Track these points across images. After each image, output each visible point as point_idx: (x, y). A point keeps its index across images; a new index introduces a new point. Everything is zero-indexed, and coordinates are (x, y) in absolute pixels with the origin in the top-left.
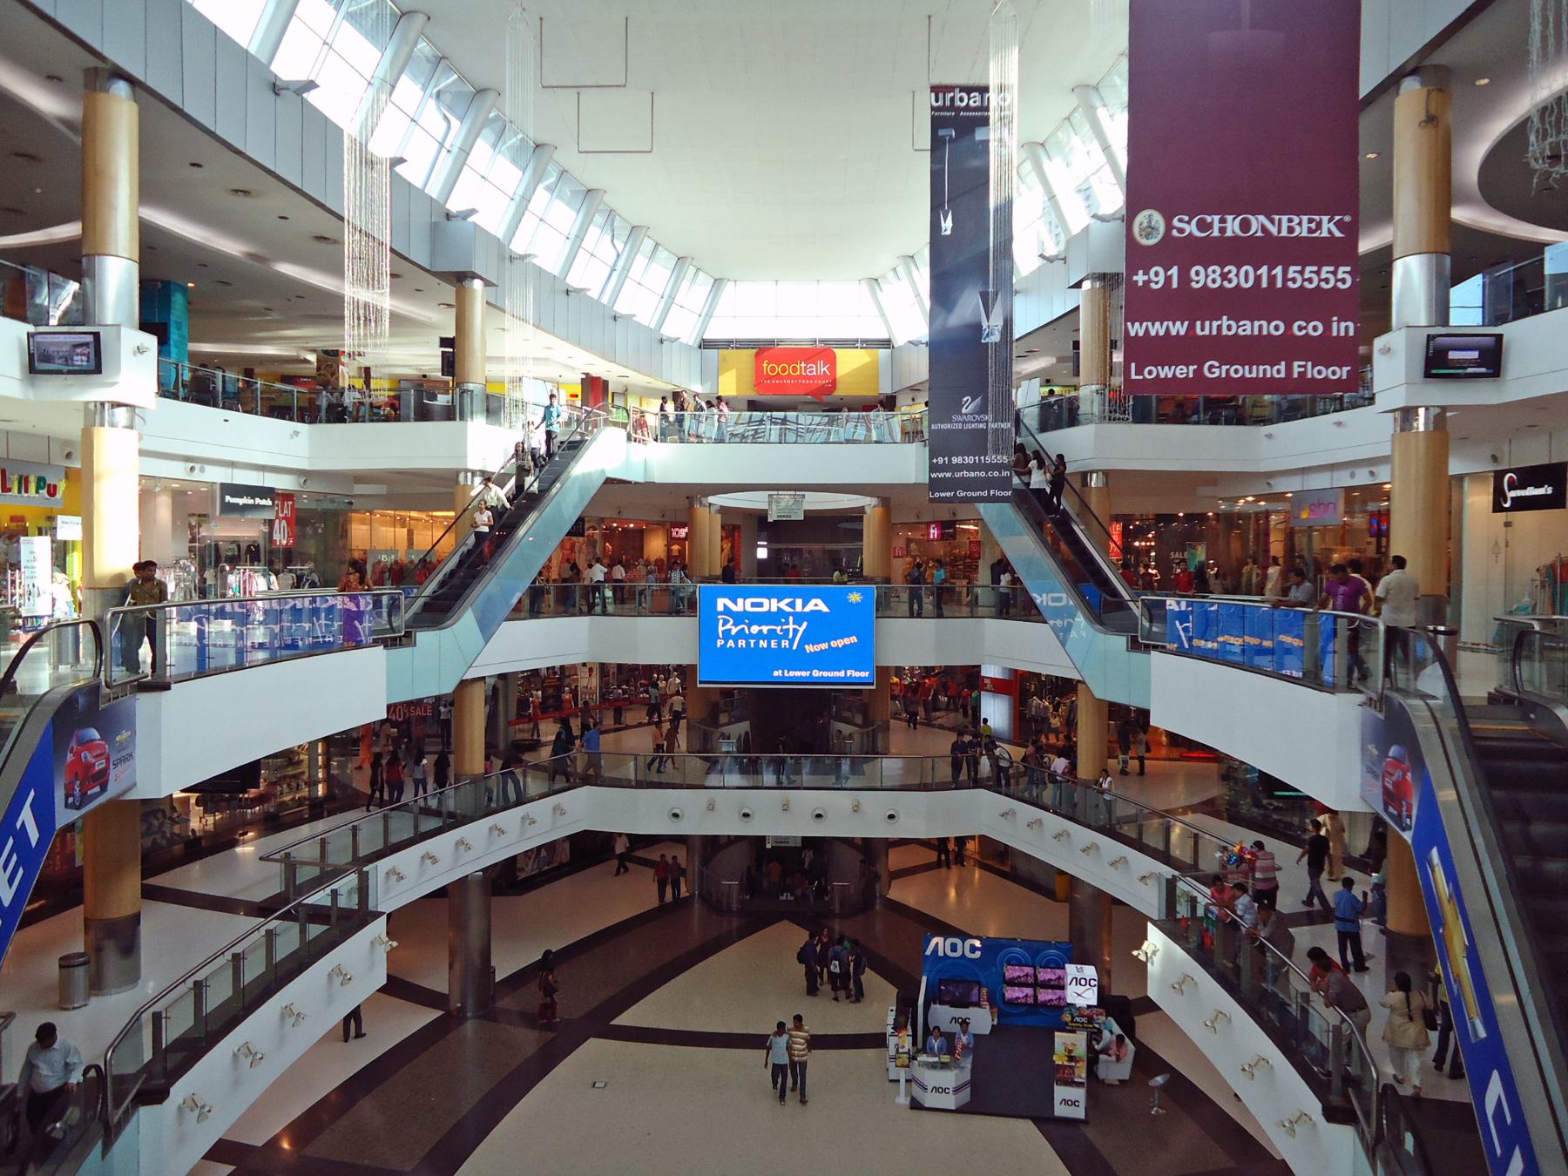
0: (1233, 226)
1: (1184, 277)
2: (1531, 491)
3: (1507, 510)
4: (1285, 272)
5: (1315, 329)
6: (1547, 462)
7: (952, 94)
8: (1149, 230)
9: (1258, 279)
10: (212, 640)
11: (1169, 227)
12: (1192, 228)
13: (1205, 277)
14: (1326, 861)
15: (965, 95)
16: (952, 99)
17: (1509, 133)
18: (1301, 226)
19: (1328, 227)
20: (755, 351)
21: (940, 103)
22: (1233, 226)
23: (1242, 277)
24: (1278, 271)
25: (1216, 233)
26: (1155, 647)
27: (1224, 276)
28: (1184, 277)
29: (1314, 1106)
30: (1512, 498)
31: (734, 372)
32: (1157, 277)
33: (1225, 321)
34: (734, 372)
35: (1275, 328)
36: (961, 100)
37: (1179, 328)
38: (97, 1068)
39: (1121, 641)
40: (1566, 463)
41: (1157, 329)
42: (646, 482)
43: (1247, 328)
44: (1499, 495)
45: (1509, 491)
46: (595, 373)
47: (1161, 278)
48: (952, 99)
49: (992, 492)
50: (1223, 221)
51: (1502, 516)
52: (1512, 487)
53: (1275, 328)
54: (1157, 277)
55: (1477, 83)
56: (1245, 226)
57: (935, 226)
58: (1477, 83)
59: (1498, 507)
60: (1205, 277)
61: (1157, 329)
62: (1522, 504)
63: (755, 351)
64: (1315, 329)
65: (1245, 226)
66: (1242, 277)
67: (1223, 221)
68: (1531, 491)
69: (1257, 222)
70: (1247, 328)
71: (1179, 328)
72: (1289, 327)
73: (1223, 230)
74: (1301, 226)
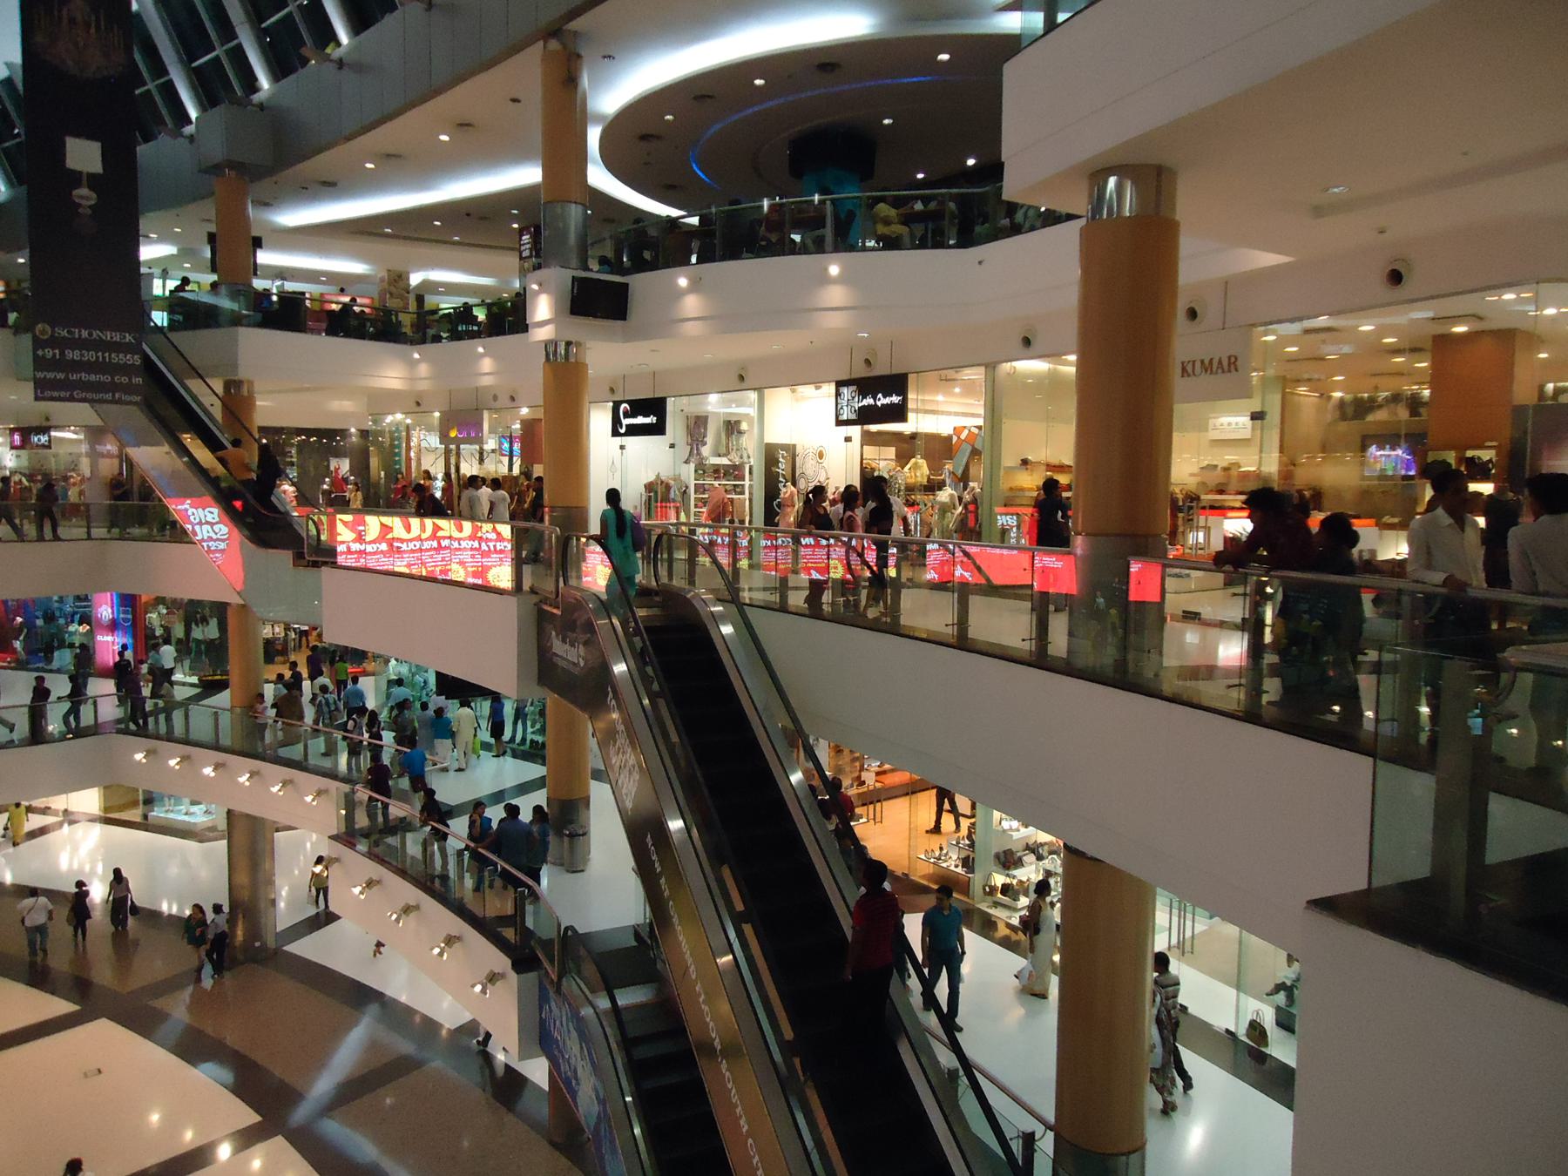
0: (85, 334)
2: (640, 420)
3: (622, 435)
4: (110, 355)
6: (652, 396)
8: (43, 332)
9: (97, 357)
10: (476, 463)
11: (53, 331)
12: (65, 333)
13: (71, 355)
14: (909, 966)
17: (650, 95)
19: (128, 338)
22: (85, 334)
23: (90, 356)
24: (107, 354)
25: (77, 336)
26: (325, 563)
27: (82, 355)
28: (62, 353)
30: (627, 426)
32: (49, 353)
33: (83, 374)
35: (107, 378)
39: (286, 556)
41: (50, 375)
42: (374, 1090)
43: (93, 378)
44: (616, 422)
47: (51, 353)
49: (117, 396)
50: (80, 331)
51: (618, 440)
52: (626, 415)
53: (107, 378)
59: (615, 433)
60: (71, 355)
61: (50, 375)
62: (634, 431)
64: (124, 380)
65: (90, 334)
66: (90, 356)
67: (80, 331)
68: (640, 420)
69: (96, 334)
70: (93, 378)
72: (113, 379)
73: (80, 335)
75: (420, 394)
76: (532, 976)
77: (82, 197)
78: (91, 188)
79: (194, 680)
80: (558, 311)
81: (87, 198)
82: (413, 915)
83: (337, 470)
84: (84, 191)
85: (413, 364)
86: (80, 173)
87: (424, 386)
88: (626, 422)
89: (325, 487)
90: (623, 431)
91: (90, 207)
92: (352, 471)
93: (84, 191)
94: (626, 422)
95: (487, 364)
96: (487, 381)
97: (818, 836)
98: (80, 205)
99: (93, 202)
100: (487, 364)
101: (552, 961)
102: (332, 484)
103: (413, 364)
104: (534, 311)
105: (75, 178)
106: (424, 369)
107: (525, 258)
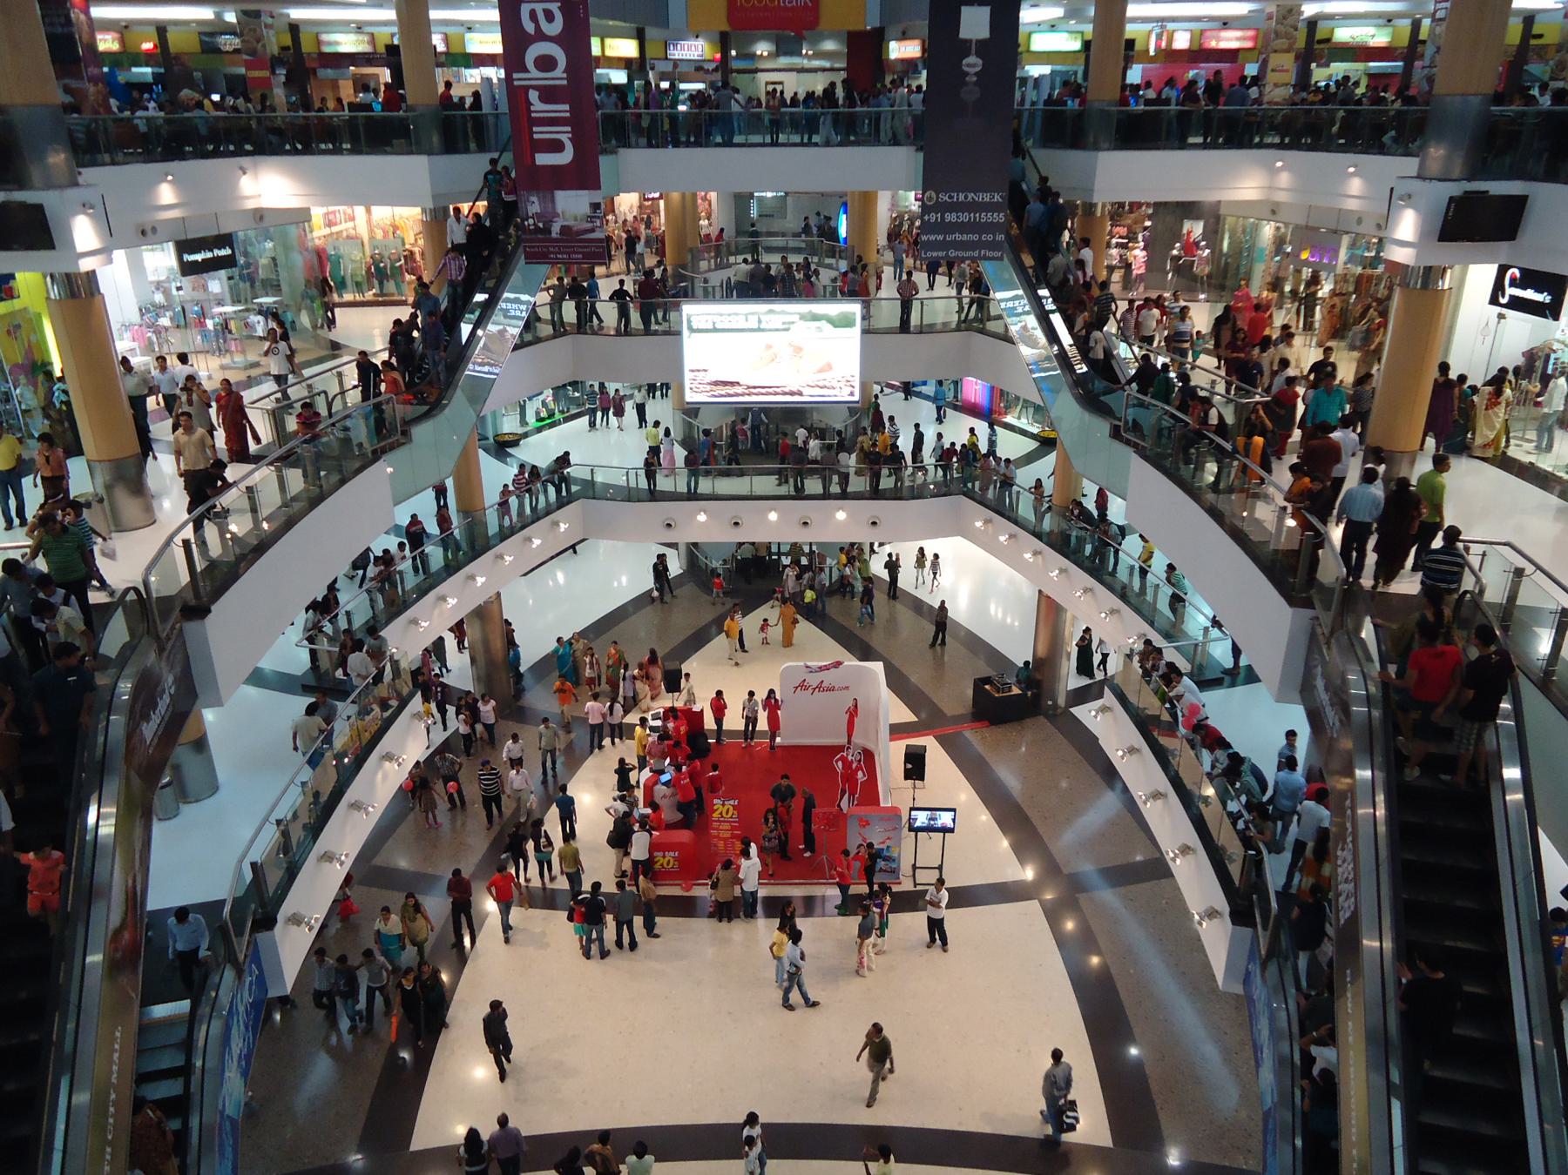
0: (962, 197)
1: (943, 217)
2: (1530, 294)
5: (990, 237)
7: (533, 96)
8: (930, 198)
13: (950, 217)
15: (534, 51)
16: (548, 94)
18: (987, 197)
20: (68, 99)
21: (538, 106)
23: (965, 217)
28: (943, 217)
29: (1222, 905)
31: (412, 1149)
32: (933, 217)
34: (412, 1149)
35: (975, 237)
36: (546, 63)
37: (940, 238)
38: (136, 590)
40: (1563, 277)
41: (932, 238)
43: (965, 237)
44: (1498, 287)
45: (1511, 285)
46: (15, 301)
48: (548, 94)
51: (1498, 309)
52: (1513, 283)
53: (975, 237)
54: (933, 217)
55: (486, 296)
56: (966, 197)
57: (718, 145)
58: (486, 296)
59: (1494, 301)
60: (950, 217)
61: (932, 238)
62: (1517, 304)
63: (68, 99)
64: (990, 237)
65: (966, 197)
66: (965, 217)
68: (1530, 294)
69: (970, 196)
70: (965, 237)
71: (940, 238)
74: (987, 197)
75: (1277, 204)
76: (1247, 932)
77: (969, 65)
78: (978, 55)
79: (1035, 430)
80: (1423, 234)
81: (973, 66)
82: (1159, 802)
83: (1189, 233)
84: (972, 59)
85: (1274, 172)
86: (971, 41)
87: (1282, 197)
88: (1511, 291)
89: (1175, 252)
90: (1504, 301)
91: (976, 74)
92: (1205, 236)
93: (972, 59)
94: (1511, 291)
95: (1356, 186)
96: (1352, 205)
97: (1533, 1022)
98: (967, 74)
99: (978, 69)
100: (1356, 186)
101: (1265, 928)
102: (1182, 248)
103: (1274, 172)
104: (1396, 224)
105: (965, 47)
106: (1284, 179)
107: (1440, 19)
